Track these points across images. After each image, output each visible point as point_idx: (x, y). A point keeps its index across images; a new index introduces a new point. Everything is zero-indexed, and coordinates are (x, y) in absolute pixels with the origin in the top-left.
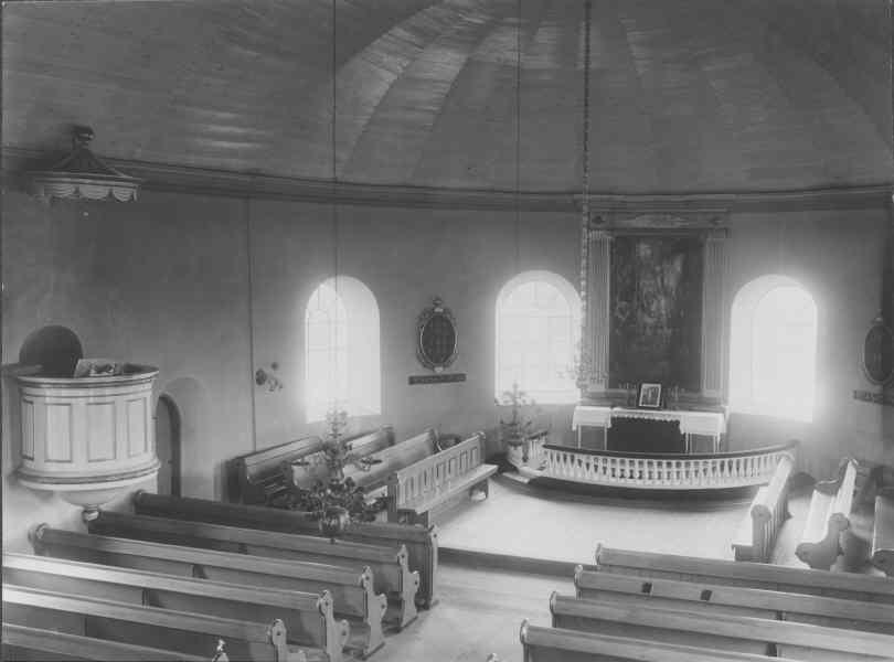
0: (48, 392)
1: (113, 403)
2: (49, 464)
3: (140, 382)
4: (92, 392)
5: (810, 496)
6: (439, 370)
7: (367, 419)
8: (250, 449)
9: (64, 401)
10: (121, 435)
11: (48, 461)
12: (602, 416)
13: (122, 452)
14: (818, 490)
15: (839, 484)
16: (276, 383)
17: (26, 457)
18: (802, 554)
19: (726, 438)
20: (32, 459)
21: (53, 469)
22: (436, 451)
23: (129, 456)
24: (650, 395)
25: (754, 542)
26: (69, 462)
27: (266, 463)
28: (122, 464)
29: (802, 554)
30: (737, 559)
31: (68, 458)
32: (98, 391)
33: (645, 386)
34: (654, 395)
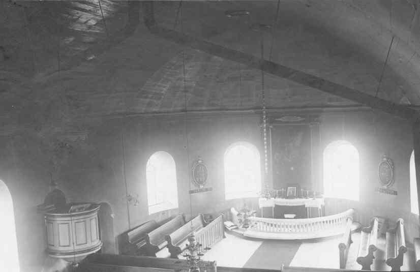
0: (58, 219)
1: (84, 221)
2: (60, 247)
3: (93, 212)
4: (75, 218)
5: (360, 232)
6: (201, 187)
7: (172, 210)
8: (128, 229)
9: (66, 222)
10: (88, 233)
11: (60, 246)
12: (271, 203)
13: (89, 241)
14: (364, 231)
15: (371, 229)
16: (137, 201)
17: (50, 245)
18: (360, 260)
19: (323, 208)
20: (53, 246)
21: (61, 249)
22: (205, 225)
23: (92, 241)
24: (291, 192)
25: (180, 203)
26: (69, 246)
27: (135, 234)
28: (89, 245)
29: (360, 260)
30: (340, 268)
31: (68, 244)
32: (78, 218)
33: (289, 188)
34: (293, 192)
